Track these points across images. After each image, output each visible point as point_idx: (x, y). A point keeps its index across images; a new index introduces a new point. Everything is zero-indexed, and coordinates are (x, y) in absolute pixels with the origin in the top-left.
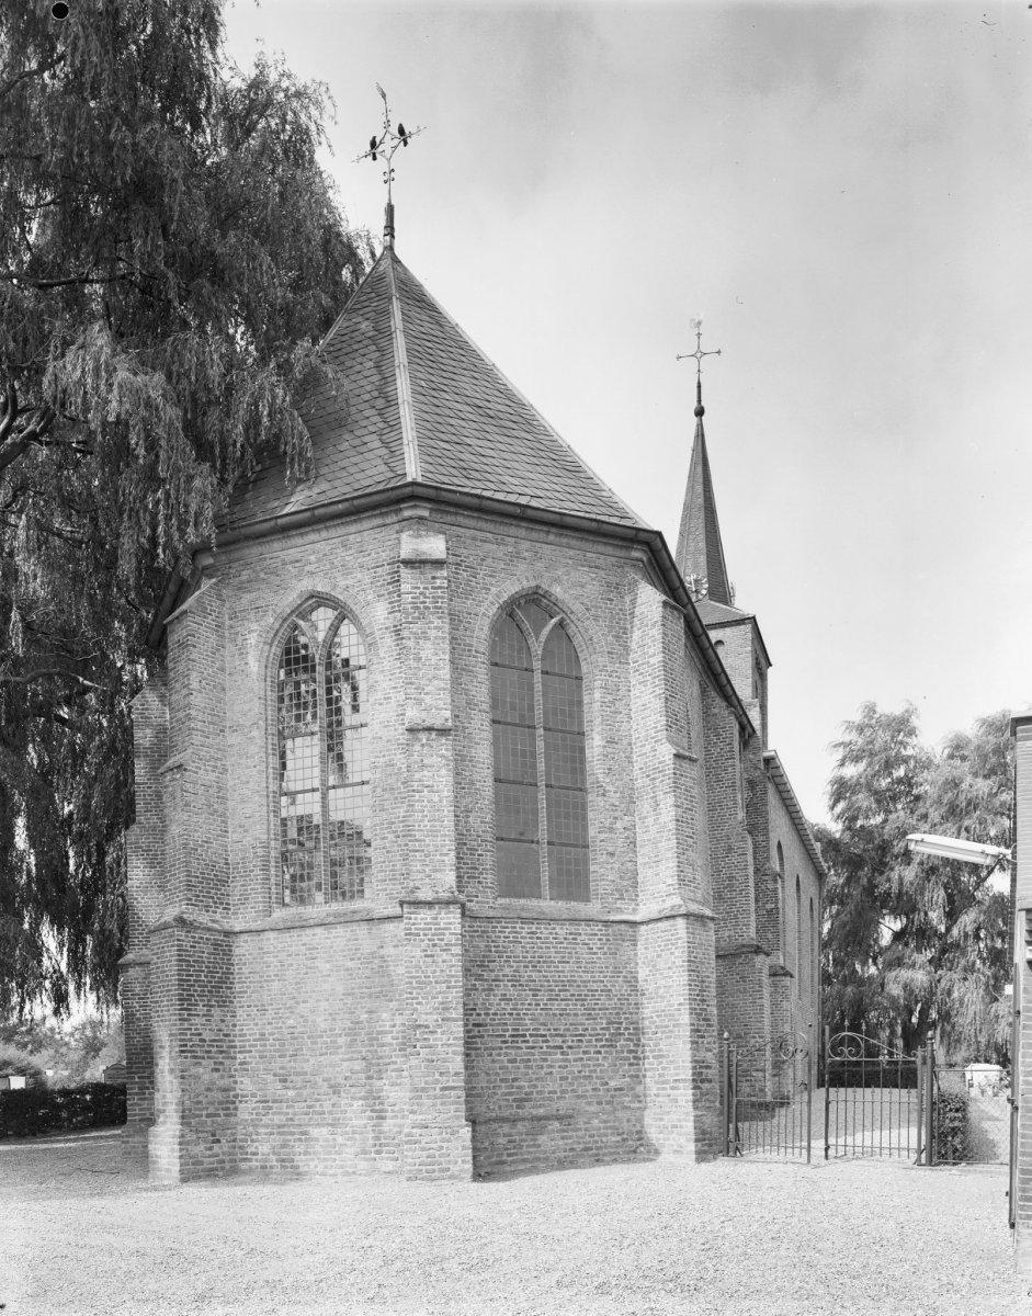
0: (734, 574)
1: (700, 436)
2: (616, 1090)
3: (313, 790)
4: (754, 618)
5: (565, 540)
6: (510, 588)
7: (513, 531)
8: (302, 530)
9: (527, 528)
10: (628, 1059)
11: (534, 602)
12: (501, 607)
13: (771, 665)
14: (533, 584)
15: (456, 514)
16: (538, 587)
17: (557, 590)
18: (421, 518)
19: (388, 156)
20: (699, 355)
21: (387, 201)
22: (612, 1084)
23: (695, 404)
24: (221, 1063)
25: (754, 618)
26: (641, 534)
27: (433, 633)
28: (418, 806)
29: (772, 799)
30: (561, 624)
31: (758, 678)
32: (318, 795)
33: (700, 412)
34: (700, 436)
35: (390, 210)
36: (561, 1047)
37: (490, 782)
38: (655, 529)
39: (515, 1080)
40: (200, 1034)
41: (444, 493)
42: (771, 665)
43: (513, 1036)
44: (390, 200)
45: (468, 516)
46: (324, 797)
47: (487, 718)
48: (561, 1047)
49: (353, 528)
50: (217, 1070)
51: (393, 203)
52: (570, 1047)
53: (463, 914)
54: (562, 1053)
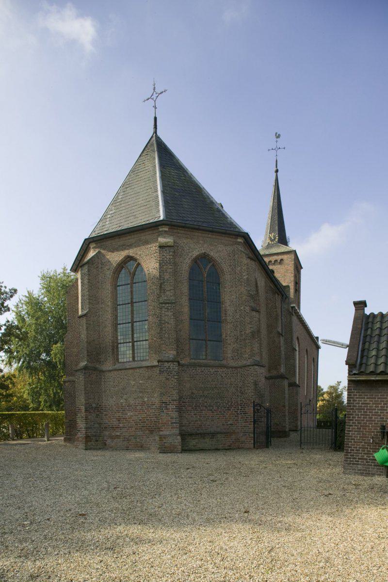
0: (288, 233)
1: (277, 180)
2: (230, 425)
3: (129, 303)
4: (295, 251)
5: (214, 236)
6: (196, 253)
7: (196, 234)
8: (126, 235)
9: (201, 233)
10: (234, 414)
11: (204, 258)
12: (192, 260)
13: (302, 268)
14: (203, 252)
15: (177, 229)
16: (205, 253)
17: (212, 254)
18: (166, 231)
19: (155, 99)
20: (277, 149)
21: (154, 116)
22: (229, 423)
23: (275, 169)
24: (98, 415)
25: (295, 251)
26: (240, 233)
27: (169, 270)
28: (164, 329)
29: (294, 318)
30: (213, 265)
31: (296, 273)
32: (130, 325)
33: (277, 171)
34: (277, 180)
35: (155, 119)
36: (212, 410)
37: (188, 320)
38: (246, 232)
39: (196, 421)
40: (91, 405)
41: (173, 223)
42: (302, 268)
43: (195, 406)
44: (155, 132)
45: (181, 230)
46: (132, 325)
47: (187, 298)
48: (212, 410)
49: (142, 234)
50: (97, 417)
51: (157, 116)
52: (215, 410)
53: (179, 365)
54: (212, 412)
